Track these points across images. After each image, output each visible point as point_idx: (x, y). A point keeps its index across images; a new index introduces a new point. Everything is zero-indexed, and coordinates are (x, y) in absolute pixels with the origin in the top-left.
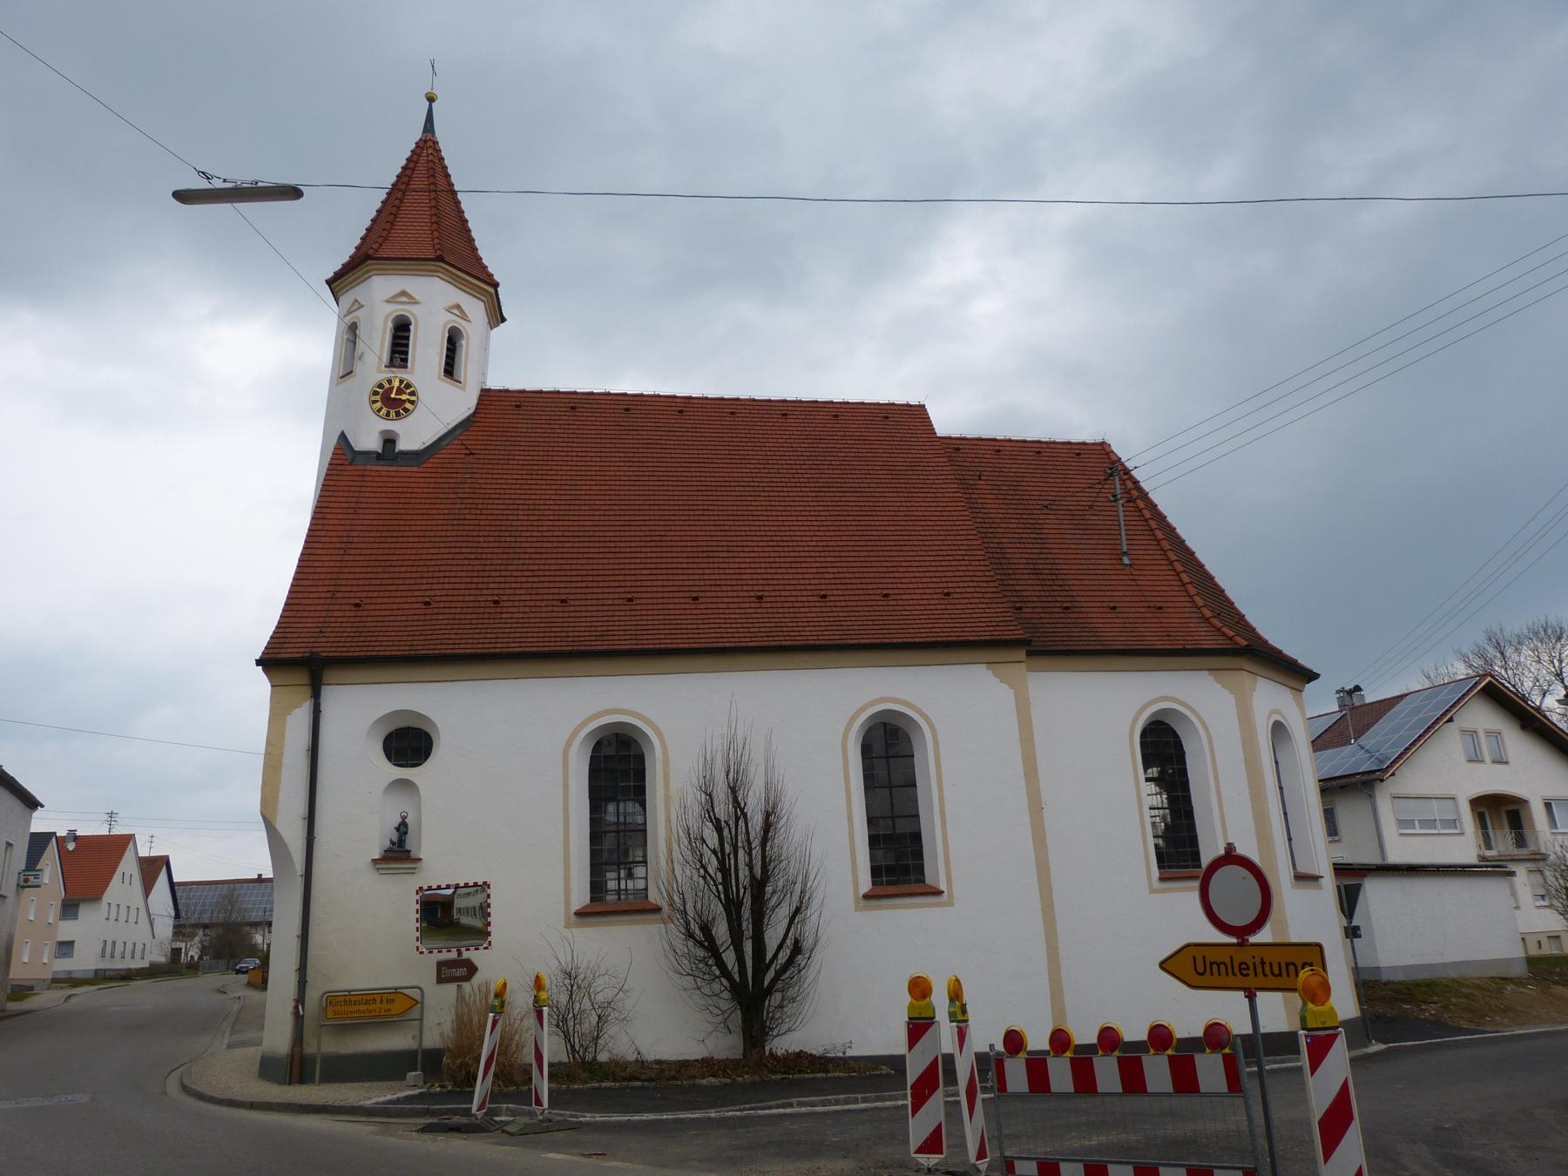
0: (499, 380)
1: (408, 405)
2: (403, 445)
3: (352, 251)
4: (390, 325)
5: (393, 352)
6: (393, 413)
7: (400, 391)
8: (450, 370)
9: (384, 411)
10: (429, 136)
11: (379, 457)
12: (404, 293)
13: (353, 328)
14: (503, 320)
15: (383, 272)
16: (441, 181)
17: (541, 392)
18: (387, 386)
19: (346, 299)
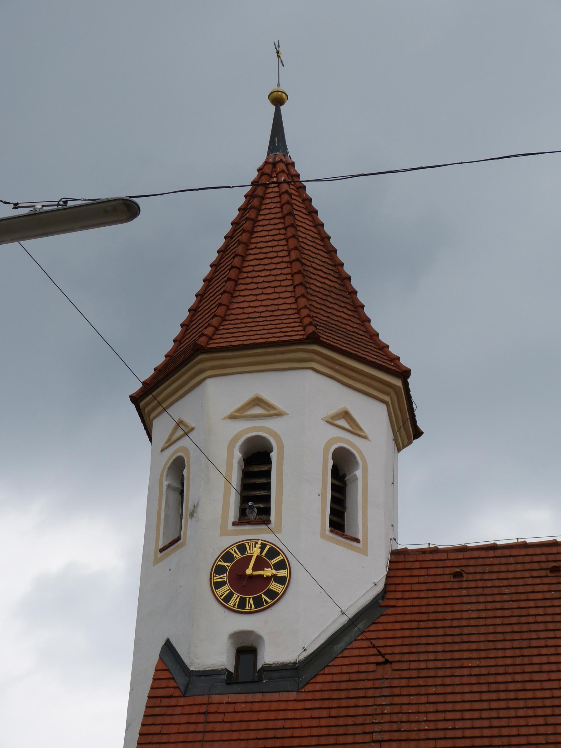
0: (419, 532)
1: (275, 586)
2: (270, 655)
3: (169, 346)
4: (238, 455)
5: (244, 499)
6: (250, 602)
7: (260, 564)
8: (339, 521)
9: (235, 599)
10: (279, 156)
11: (229, 679)
12: (258, 401)
13: (178, 467)
14: (418, 433)
15: (224, 371)
16: (301, 219)
17: (493, 547)
18: (238, 556)
19: (163, 425)
